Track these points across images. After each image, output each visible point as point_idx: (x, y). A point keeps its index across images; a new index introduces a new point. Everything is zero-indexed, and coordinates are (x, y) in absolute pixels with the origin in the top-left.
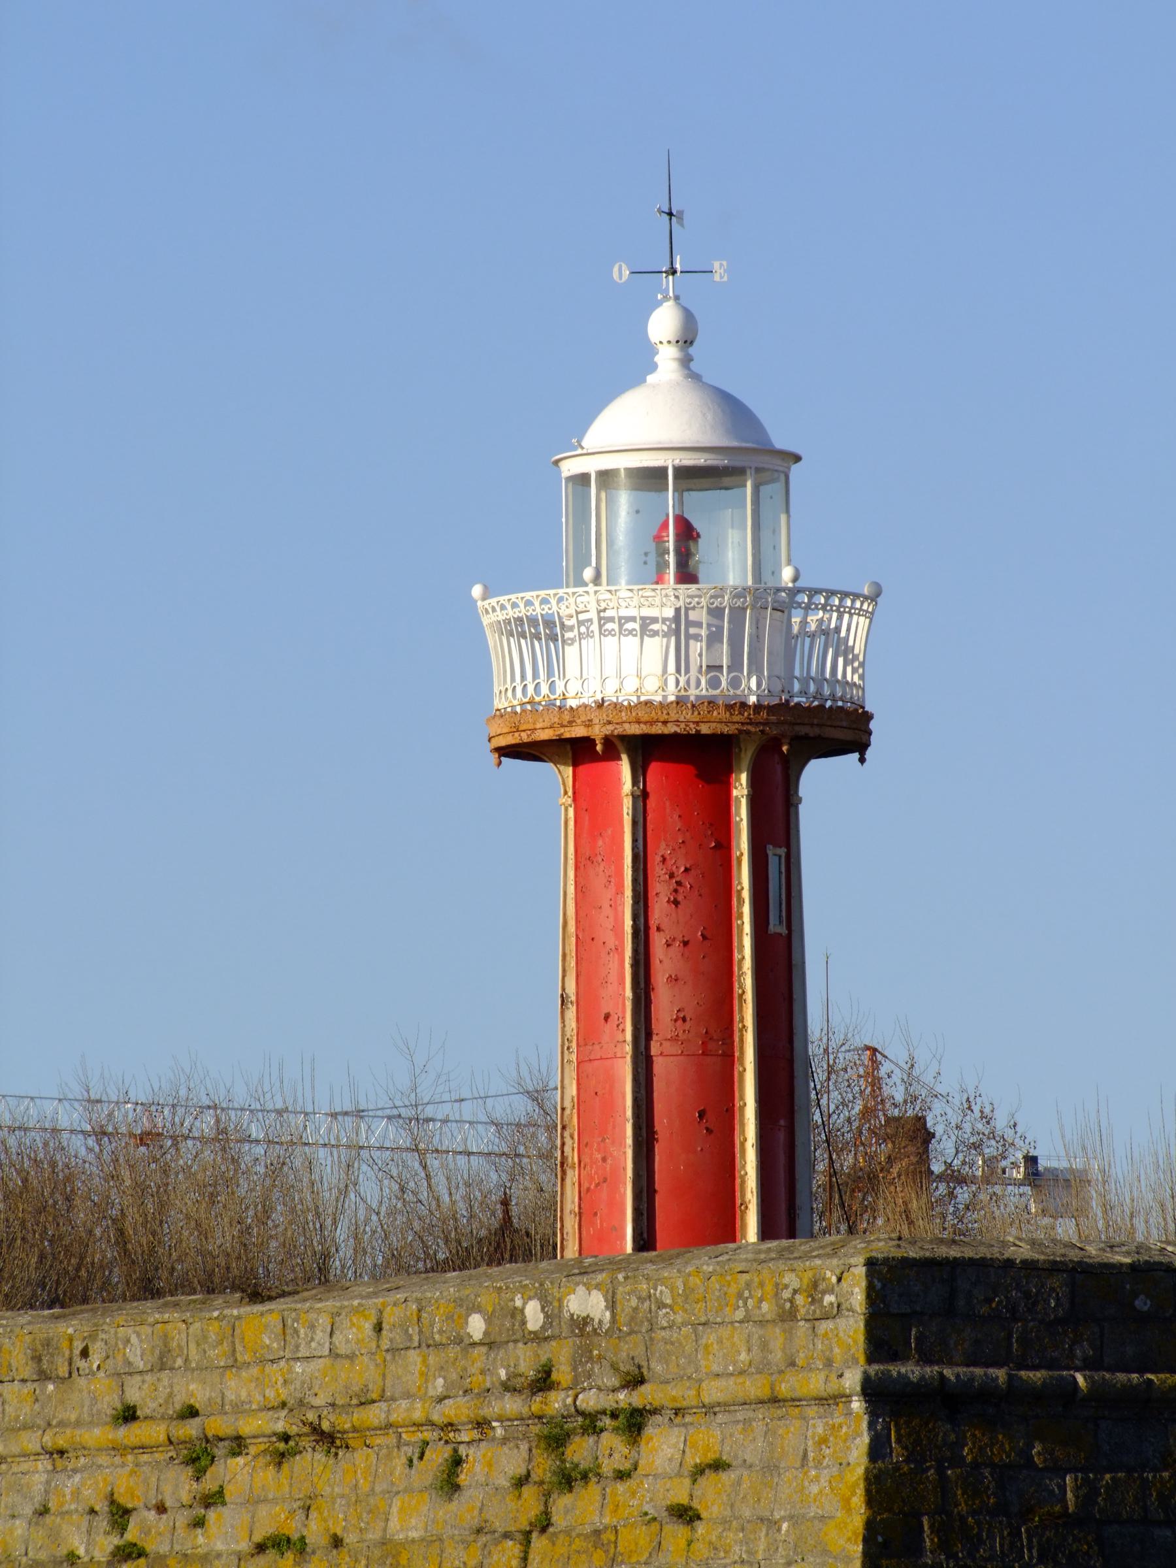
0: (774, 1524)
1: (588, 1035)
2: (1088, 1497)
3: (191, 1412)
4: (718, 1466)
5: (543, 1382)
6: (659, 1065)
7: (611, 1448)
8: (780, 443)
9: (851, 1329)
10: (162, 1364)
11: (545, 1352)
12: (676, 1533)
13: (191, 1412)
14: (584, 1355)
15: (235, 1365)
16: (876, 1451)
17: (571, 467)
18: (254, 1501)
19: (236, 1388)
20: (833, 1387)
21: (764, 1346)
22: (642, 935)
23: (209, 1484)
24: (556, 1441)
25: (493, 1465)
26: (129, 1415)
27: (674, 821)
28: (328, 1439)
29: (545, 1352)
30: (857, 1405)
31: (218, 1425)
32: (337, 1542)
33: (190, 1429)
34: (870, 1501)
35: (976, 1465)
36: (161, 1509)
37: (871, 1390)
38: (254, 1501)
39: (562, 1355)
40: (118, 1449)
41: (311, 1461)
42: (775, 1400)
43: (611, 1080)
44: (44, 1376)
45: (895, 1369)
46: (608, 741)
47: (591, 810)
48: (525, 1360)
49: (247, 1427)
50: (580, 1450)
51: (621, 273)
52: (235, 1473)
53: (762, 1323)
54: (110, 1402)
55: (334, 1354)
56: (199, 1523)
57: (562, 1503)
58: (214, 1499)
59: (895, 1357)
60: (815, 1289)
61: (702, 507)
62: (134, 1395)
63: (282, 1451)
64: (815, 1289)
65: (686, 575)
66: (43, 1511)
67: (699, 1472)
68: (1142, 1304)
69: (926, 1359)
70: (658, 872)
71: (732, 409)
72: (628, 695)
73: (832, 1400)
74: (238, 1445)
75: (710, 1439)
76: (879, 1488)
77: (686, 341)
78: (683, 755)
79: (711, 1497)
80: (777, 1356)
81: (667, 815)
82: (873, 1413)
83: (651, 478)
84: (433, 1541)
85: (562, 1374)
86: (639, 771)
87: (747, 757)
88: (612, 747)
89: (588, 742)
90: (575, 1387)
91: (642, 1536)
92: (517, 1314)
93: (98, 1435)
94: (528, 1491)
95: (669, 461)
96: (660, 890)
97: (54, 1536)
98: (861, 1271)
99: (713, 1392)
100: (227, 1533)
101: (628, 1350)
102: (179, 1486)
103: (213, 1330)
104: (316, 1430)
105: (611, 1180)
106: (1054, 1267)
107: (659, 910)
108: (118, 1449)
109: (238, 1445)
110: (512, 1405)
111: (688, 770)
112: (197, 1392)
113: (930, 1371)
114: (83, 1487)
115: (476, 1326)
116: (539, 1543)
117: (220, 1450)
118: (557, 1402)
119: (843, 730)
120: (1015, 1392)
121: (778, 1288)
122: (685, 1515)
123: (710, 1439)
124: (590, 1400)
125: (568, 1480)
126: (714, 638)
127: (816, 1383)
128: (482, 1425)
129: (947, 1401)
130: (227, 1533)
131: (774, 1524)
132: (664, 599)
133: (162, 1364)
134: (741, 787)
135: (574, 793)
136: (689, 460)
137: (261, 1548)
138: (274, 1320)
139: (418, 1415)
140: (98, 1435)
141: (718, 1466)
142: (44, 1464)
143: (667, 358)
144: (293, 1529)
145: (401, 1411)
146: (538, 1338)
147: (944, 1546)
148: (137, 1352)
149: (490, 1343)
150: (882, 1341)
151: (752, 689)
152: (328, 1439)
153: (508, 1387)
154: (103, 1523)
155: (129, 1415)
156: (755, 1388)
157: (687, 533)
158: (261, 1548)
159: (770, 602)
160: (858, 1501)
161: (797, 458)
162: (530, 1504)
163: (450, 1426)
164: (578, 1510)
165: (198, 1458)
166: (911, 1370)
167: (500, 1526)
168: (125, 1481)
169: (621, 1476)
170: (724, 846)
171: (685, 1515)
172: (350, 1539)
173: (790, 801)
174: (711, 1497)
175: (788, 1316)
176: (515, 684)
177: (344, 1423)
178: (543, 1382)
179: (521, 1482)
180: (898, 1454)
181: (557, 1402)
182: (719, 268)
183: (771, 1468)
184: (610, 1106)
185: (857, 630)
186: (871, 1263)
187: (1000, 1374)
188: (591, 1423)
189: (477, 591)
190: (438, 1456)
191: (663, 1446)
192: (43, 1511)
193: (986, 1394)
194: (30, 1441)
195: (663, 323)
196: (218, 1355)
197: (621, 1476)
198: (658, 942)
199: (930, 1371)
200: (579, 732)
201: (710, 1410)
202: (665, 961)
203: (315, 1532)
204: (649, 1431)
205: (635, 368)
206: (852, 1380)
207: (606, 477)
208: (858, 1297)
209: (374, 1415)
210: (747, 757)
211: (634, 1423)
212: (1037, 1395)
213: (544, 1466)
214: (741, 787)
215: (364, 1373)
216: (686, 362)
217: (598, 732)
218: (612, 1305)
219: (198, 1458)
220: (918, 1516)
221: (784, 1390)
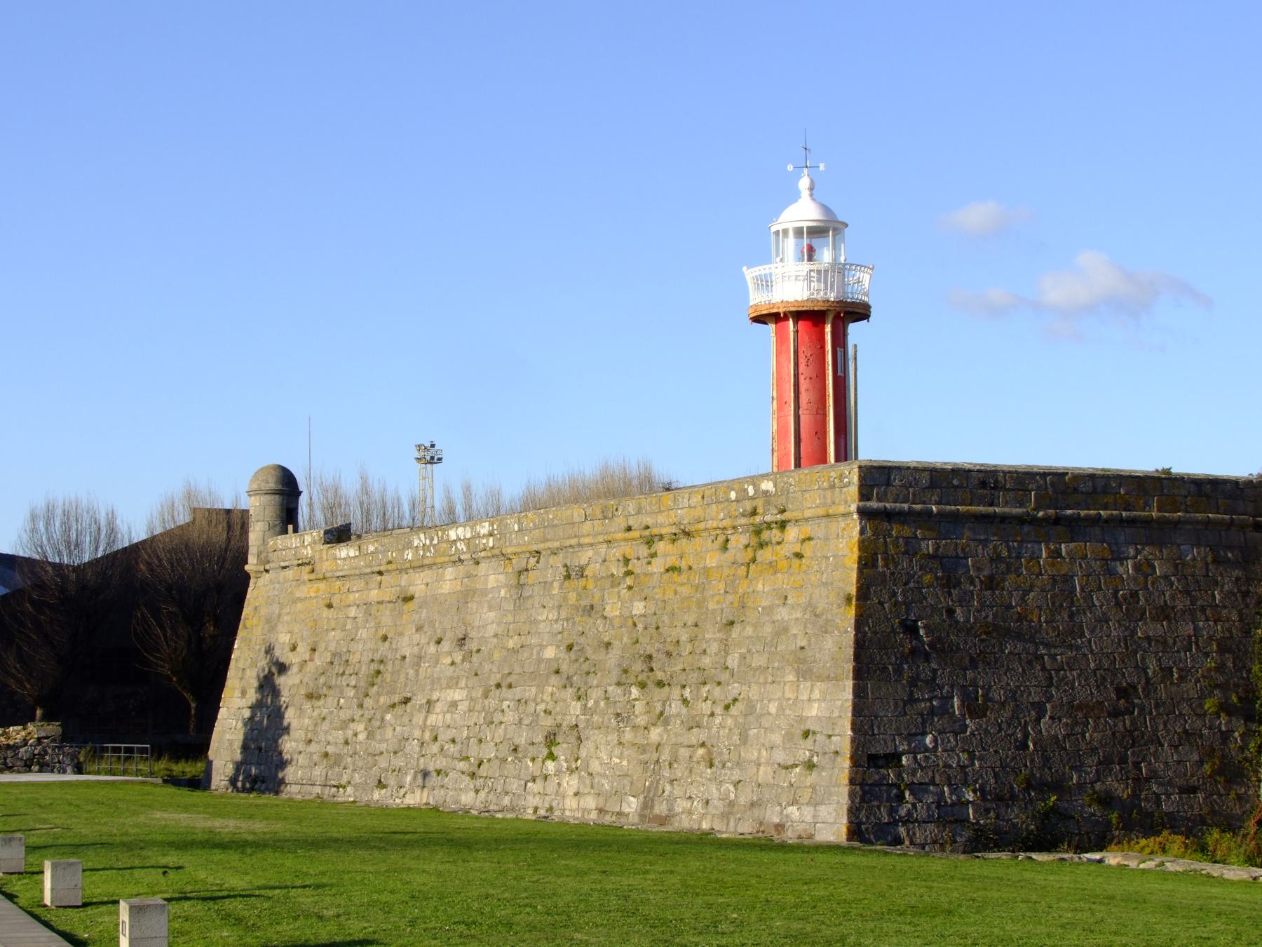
0: (828, 558)
1: (780, 409)
2: (937, 549)
3: (648, 527)
4: (809, 539)
5: (754, 513)
6: (802, 418)
7: (775, 534)
8: (840, 219)
9: (854, 490)
10: (639, 512)
11: (755, 503)
12: (796, 562)
13: (648, 527)
14: (767, 503)
15: (660, 511)
16: (862, 532)
17: (774, 229)
18: (665, 555)
19: (661, 519)
20: (847, 510)
21: (825, 497)
22: (796, 376)
23: (653, 550)
24: (758, 532)
25: (739, 540)
26: (629, 529)
27: (807, 339)
28: (687, 534)
29: (755, 503)
30: (855, 516)
31: (655, 531)
32: (690, 568)
33: (647, 533)
34: (860, 550)
35: (897, 537)
36: (638, 559)
37: (862, 512)
38: (665, 555)
39: (760, 503)
40: (626, 540)
41: (684, 541)
42: (828, 516)
43: (787, 423)
44: (605, 518)
45: (869, 504)
46: (785, 313)
47: (781, 338)
48: (748, 506)
49: (664, 531)
50: (765, 535)
51: (790, 168)
52: (661, 546)
53: (824, 489)
54: (624, 525)
55: (690, 506)
56: (649, 563)
57: (760, 553)
58: (654, 555)
59: (869, 499)
60: (841, 477)
61: (816, 242)
62: (631, 523)
63: (674, 538)
64: (841, 477)
65: (810, 259)
66: (605, 561)
67: (803, 541)
68: (955, 482)
69: (879, 500)
70: (801, 356)
71: (826, 209)
72: (791, 299)
73: (847, 515)
74: (661, 537)
75: (808, 529)
76: (863, 545)
77: (811, 189)
78: (810, 317)
79: (807, 550)
80: (829, 501)
81: (805, 338)
82: (861, 520)
83: (799, 232)
84: (719, 567)
85: (760, 510)
86: (795, 323)
87: (830, 318)
88: (786, 317)
89: (778, 314)
90: (764, 514)
91: (785, 563)
92: (746, 491)
93: (620, 536)
94: (749, 549)
95: (805, 224)
96: (802, 361)
97: (608, 568)
98: (856, 470)
99: (808, 514)
100: (658, 566)
101: (781, 501)
102: (644, 551)
103: (654, 501)
104: (683, 531)
105: (788, 454)
106: (925, 470)
107: (802, 368)
108: (626, 540)
109: (661, 537)
110: (743, 521)
111: (809, 323)
112: (649, 521)
113: (881, 505)
114: (616, 553)
115: (733, 495)
116: (752, 567)
117: (656, 539)
118: (758, 519)
119: (860, 312)
120: (911, 512)
121: (829, 477)
122: (799, 556)
123: (808, 529)
124: (768, 518)
125: (762, 545)
126: (819, 280)
127: (842, 509)
128: (734, 528)
129: (888, 515)
130: (658, 566)
131: (828, 558)
132: (805, 267)
133: (639, 512)
134: (828, 329)
135: (1143, 870)
136: (811, 224)
137: (667, 570)
138: (671, 496)
139: (715, 525)
140: (620, 536)
141: (809, 539)
142: (605, 546)
143: (805, 194)
144: (677, 564)
145: (711, 524)
146: (752, 498)
147: (886, 565)
148: (631, 509)
149: (737, 501)
150: (864, 495)
151: (832, 297)
152: (687, 534)
153: (743, 515)
154: (621, 564)
155: (629, 529)
156: (821, 512)
157: (811, 250)
158: (667, 570)
159: (840, 270)
160: (856, 549)
161: (847, 226)
162: (749, 554)
163: (725, 528)
164: (765, 555)
165: (649, 542)
166: (874, 504)
167: (740, 561)
168: (628, 550)
169: (779, 543)
170: (823, 347)
171: (799, 556)
172: (694, 567)
173: (845, 335)
174: (807, 550)
175: (832, 487)
176: (759, 299)
177: (693, 529)
178: (754, 513)
179: (747, 546)
180: (869, 533)
181: (758, 519)
182: (822, 167)
183: (827, 539)
184: (787, 431)
185: (866, 278)
186: (860, 467)
187: (906, 506)
188: (769, 526)
189: (744, 268)
190: (721, 539)
191: (792, 533)
192: (605, 561)
193: (900, 513)
194: (601, 539)
195: (804, 183)
196: (655, 508)
197: (779, 543)
198: (802, 378)
199: (881, 505)
200: (775, 311)
201: (807, 520)
202: (804, 384)
203: (684, 565)
204: (788, 528)
205: (795, 196)
206: (853, 508)
207: (785, 232)
208: (855, 479)
209: (702, 526)
210: (830, 318)
211: (783, 525)
212: (919, 513)
213: (754, 541)
214: (828, 329)
215: (699, 512)
216: (811, 195)
217: (781, 310)
218: (775, 486)
219: (649, 542)
220: (876, 554)
221: (831, 512)
